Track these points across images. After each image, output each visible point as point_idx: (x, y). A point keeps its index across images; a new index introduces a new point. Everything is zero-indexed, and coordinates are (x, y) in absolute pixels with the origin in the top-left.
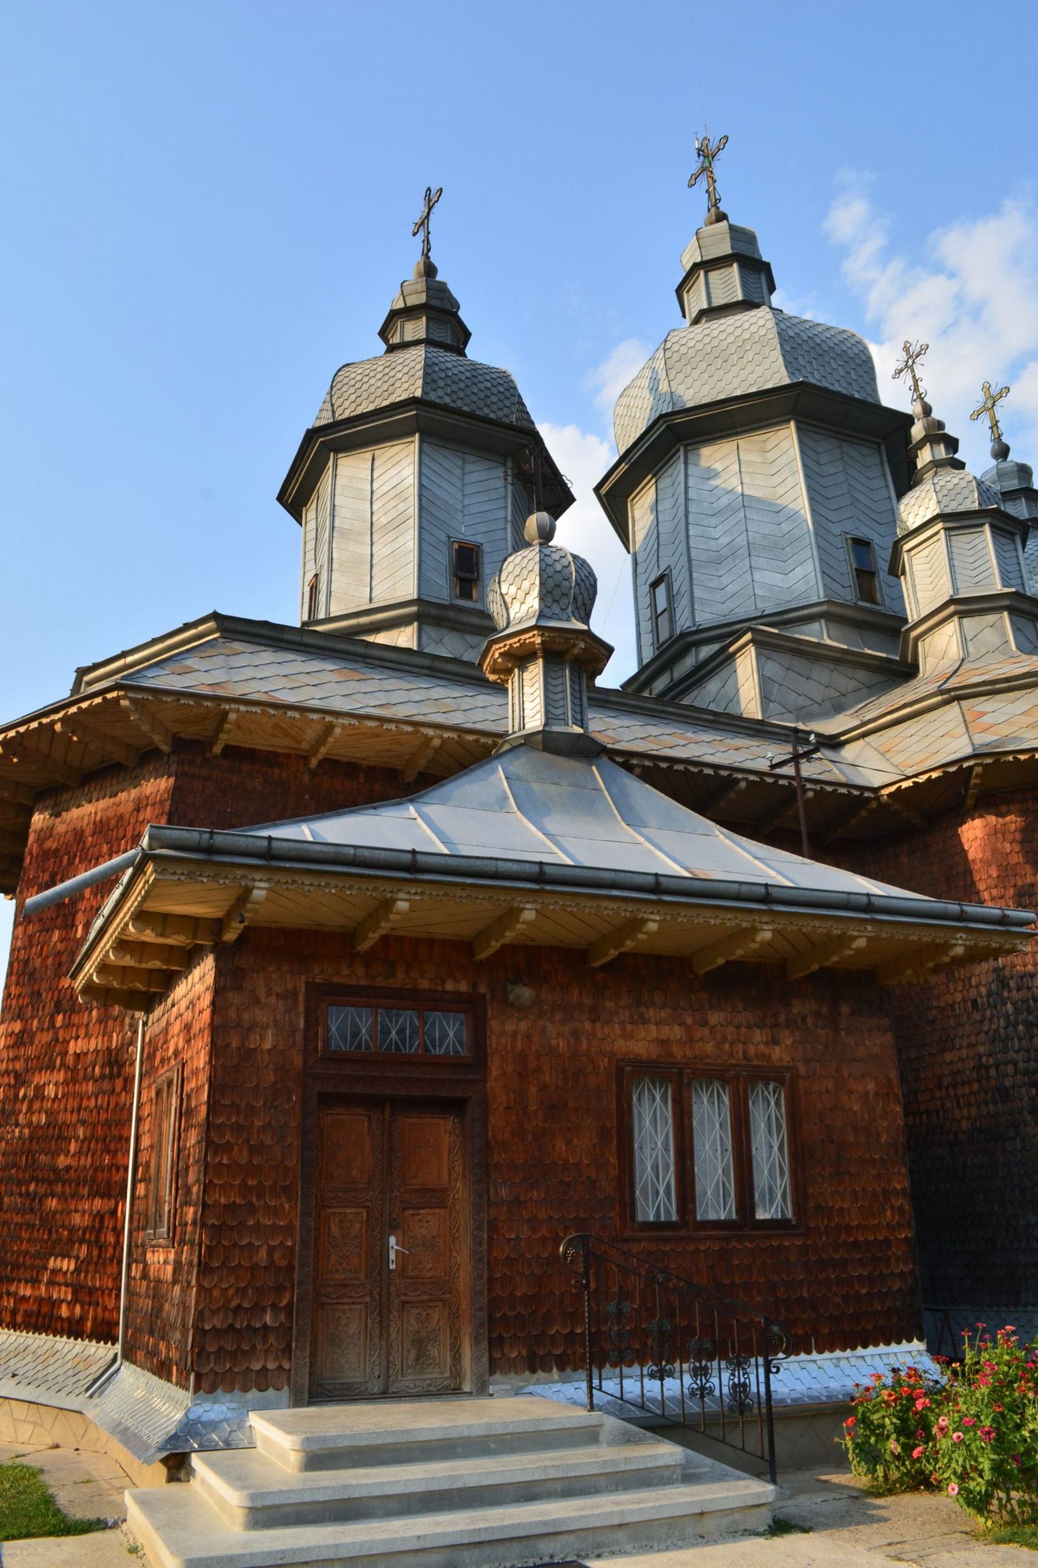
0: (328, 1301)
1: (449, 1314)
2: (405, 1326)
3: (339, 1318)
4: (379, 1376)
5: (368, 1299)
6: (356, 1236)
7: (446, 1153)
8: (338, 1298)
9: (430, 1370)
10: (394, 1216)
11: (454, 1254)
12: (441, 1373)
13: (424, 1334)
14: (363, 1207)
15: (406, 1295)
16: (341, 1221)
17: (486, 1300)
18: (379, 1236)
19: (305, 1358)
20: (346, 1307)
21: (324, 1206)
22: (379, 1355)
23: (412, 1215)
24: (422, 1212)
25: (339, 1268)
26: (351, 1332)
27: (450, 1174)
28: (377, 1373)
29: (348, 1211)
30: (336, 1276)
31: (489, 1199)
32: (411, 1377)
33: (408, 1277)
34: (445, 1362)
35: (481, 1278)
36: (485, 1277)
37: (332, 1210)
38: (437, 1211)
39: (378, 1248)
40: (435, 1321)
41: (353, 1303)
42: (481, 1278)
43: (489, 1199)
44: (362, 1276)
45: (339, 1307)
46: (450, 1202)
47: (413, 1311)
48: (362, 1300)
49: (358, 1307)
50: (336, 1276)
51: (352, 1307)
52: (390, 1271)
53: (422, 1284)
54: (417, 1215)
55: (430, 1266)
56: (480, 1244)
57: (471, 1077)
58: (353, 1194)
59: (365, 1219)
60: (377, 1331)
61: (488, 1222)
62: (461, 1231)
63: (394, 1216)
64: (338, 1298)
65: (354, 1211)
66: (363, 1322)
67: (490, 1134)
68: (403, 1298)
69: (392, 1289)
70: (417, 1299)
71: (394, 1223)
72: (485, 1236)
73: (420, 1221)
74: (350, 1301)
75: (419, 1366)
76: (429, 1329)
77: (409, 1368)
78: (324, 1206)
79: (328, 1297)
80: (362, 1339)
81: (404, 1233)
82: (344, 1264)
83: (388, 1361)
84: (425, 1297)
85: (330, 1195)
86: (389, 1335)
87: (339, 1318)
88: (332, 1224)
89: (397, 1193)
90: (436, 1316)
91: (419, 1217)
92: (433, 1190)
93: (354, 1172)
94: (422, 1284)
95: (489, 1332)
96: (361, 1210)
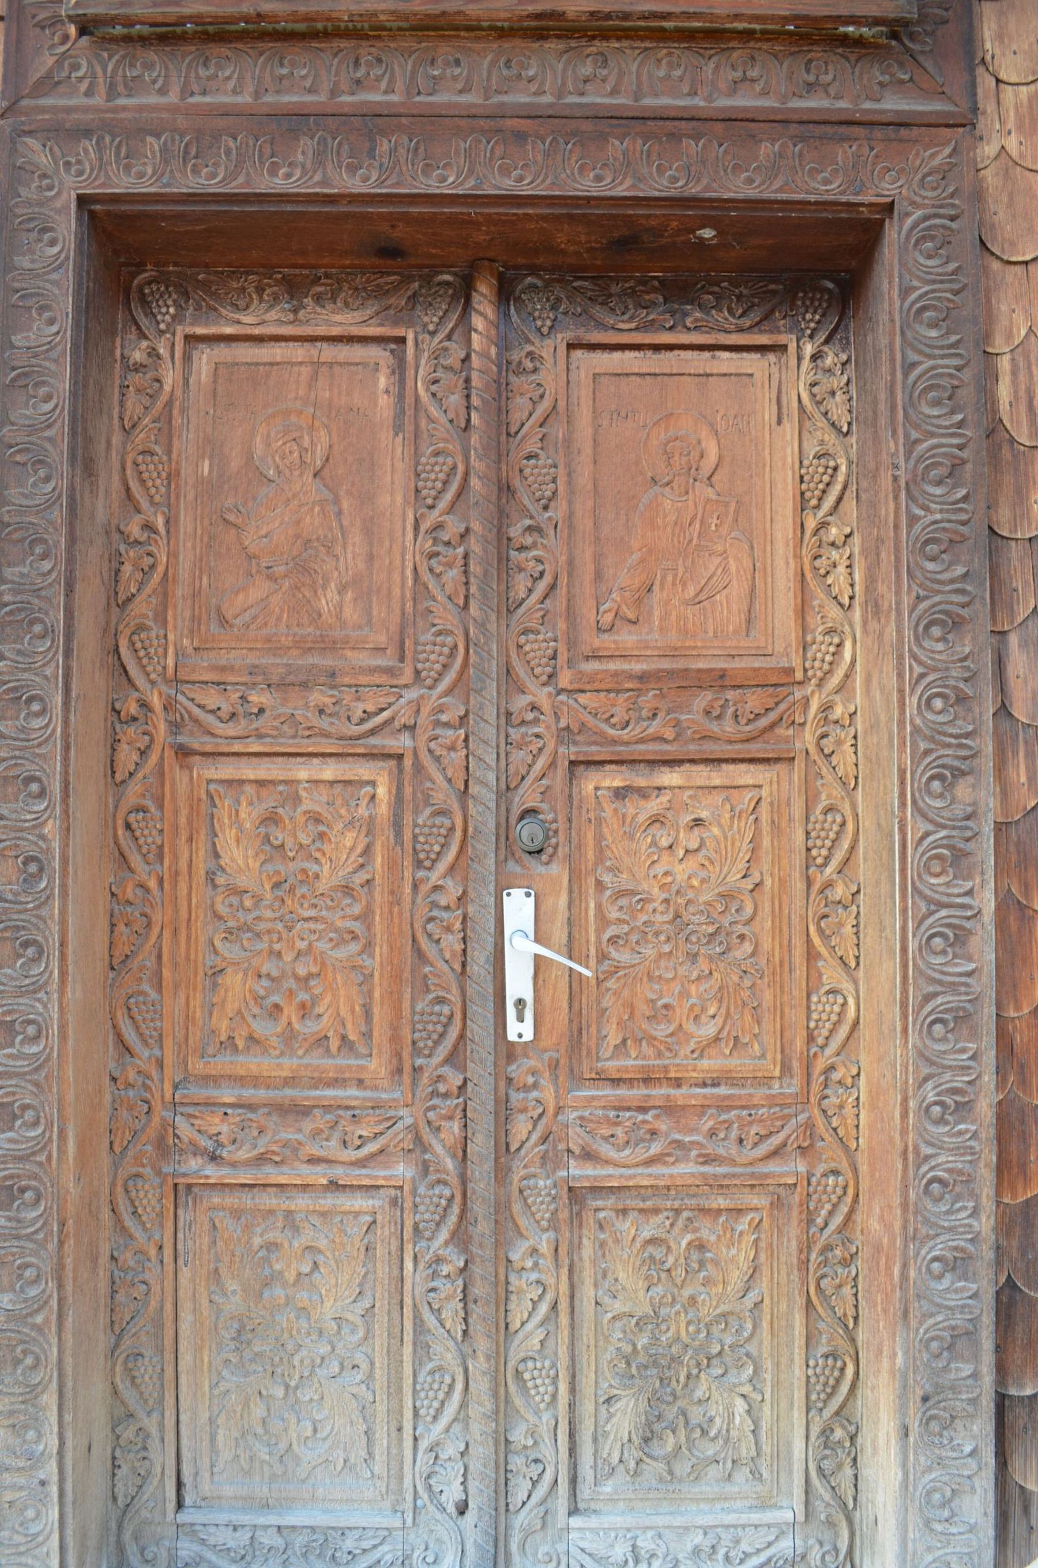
0: (213, 1173)
1: (806, 1247)
2: (587, 1292)
3: (271, 1246)
4: (462, 1509)
5: (403, 1171)
6: (347, 890)
7: (786, 508)
8: (261, 1159)
9: (708, 1487)
10: (527, 796)
11: (831, 974)
12: (764, 1504)
13: (679, 1327)
14: (370, 756)
15: (588, 1156)
16: (271, 819)
17: (986, 1224)
18: (453, 889)
19: (35, 1460)
20: (301, 1202)
21: (184, 753)
22: (462, 1416)
23: (620, 794)
24: (670, 777)
25: (261, 1028)
26: (329, 1309)
27: (802, 611)
28: (453, 1494)
29: (303, 772)
30: (252, 1063)
31: (1003, 711)
32: (618, 1520)
33: (602, 1078)
34: (781, 1455)
35: (964, 1109)
36: (985, 1107)
37: (226, 770)
38: (745, 775)
39: (452, 942)
40: (736, 1277)
41: (334, 1186)
42: (964, 1109)
43: (1003, 711)
44: (377, 1066)
45: (268, 1200)
46: (809, 737)
47: (626, 1226)
48: (378, 1174)
49: (360, 1202)
50: (252, 1063)
51: (328, 1201)
52: (510, 1052)
53: (670, 1109)
54: (643, 793)
55: (709, 1030)
56: (959, 938)
57: (893, 104)
58: (319, 697)
59: (383, 809)
60: (452, 1310)
61: (1000, 828)
62: (864, 869)
63: (527, 796)
64: (261, 1159)
65: (329, 771)
66: (383, 1270)
67: (1004, 391)
68: (579, 1172)
69: (521, 1127)
70: (643, 1176)
71: (527, 832)
72: (987, 901)
73: (656, 820)
74: (319, 1175)
75: (653, 1468)
76: (707, 1310)
77: (605, 1471)
78: (184, 753)
79: (214, 1158)
80: (380, 1341)
81: (575, 877)
82: (290, 1012)
83: (504, 1444)
84: (686, 1169)
85: (212, 699)
86: (506, 1330)
87: (271, 1246)
88: (227, 838)
89: (542, 696)
90: (741, 1255)
91: (654, 805)
92: (720, 680)
93: (327, 601)
94: (670, 1109)
95: (1001, 1369)
96: (364, 770)
